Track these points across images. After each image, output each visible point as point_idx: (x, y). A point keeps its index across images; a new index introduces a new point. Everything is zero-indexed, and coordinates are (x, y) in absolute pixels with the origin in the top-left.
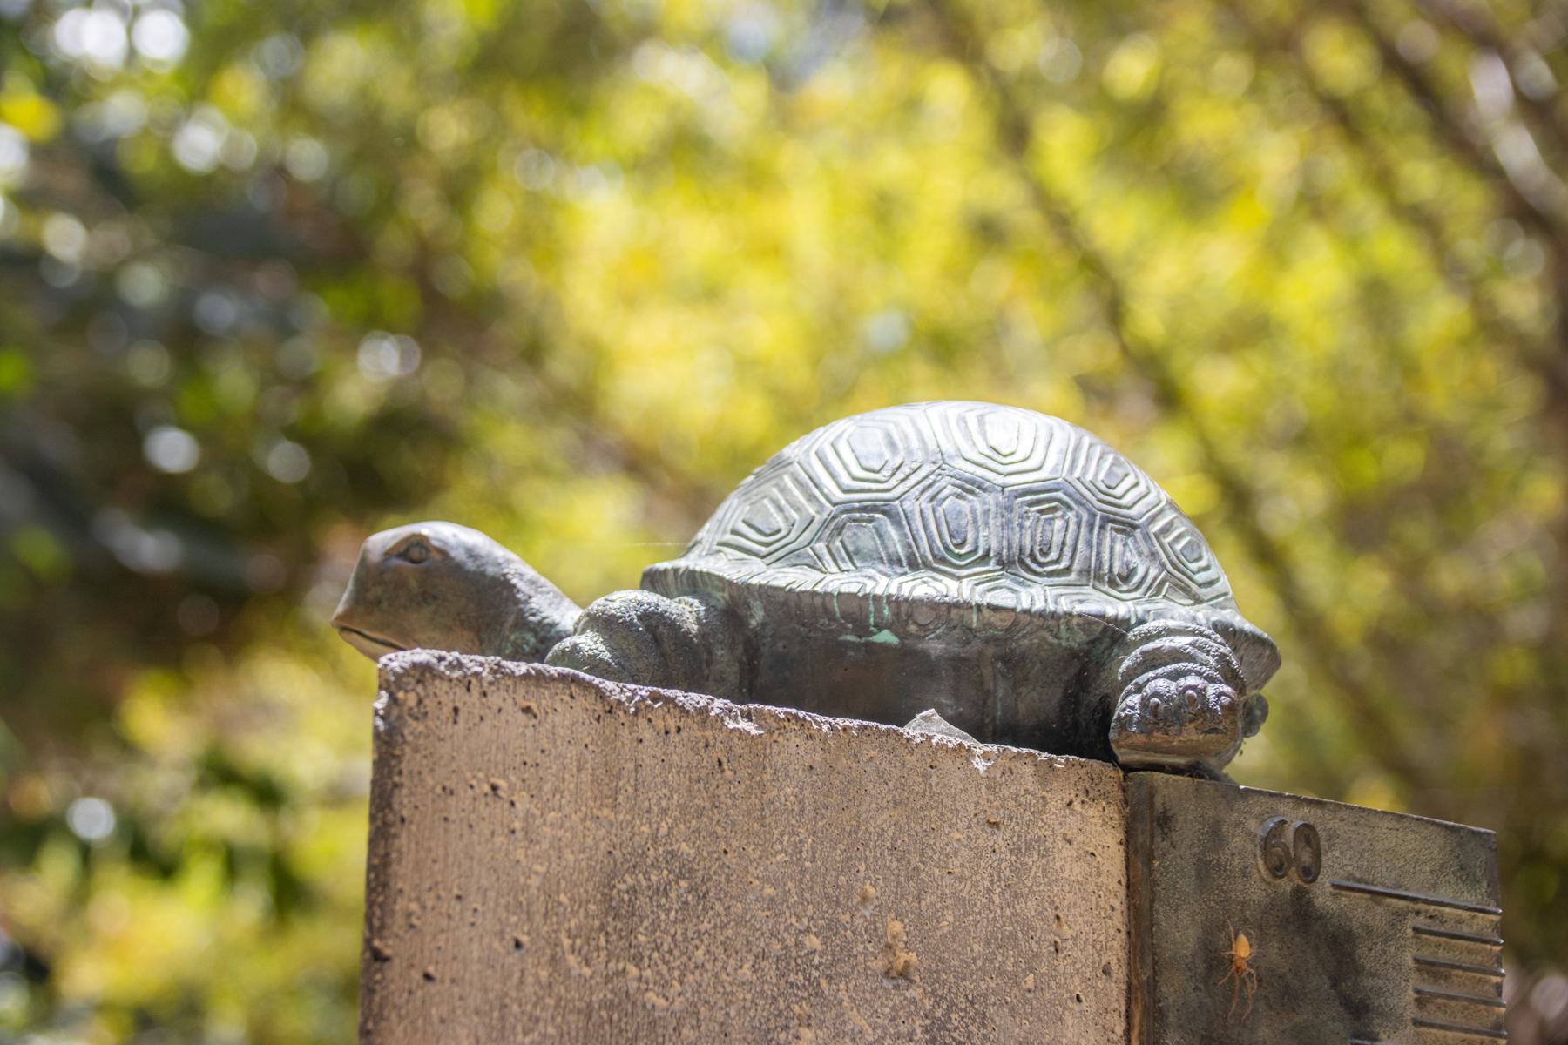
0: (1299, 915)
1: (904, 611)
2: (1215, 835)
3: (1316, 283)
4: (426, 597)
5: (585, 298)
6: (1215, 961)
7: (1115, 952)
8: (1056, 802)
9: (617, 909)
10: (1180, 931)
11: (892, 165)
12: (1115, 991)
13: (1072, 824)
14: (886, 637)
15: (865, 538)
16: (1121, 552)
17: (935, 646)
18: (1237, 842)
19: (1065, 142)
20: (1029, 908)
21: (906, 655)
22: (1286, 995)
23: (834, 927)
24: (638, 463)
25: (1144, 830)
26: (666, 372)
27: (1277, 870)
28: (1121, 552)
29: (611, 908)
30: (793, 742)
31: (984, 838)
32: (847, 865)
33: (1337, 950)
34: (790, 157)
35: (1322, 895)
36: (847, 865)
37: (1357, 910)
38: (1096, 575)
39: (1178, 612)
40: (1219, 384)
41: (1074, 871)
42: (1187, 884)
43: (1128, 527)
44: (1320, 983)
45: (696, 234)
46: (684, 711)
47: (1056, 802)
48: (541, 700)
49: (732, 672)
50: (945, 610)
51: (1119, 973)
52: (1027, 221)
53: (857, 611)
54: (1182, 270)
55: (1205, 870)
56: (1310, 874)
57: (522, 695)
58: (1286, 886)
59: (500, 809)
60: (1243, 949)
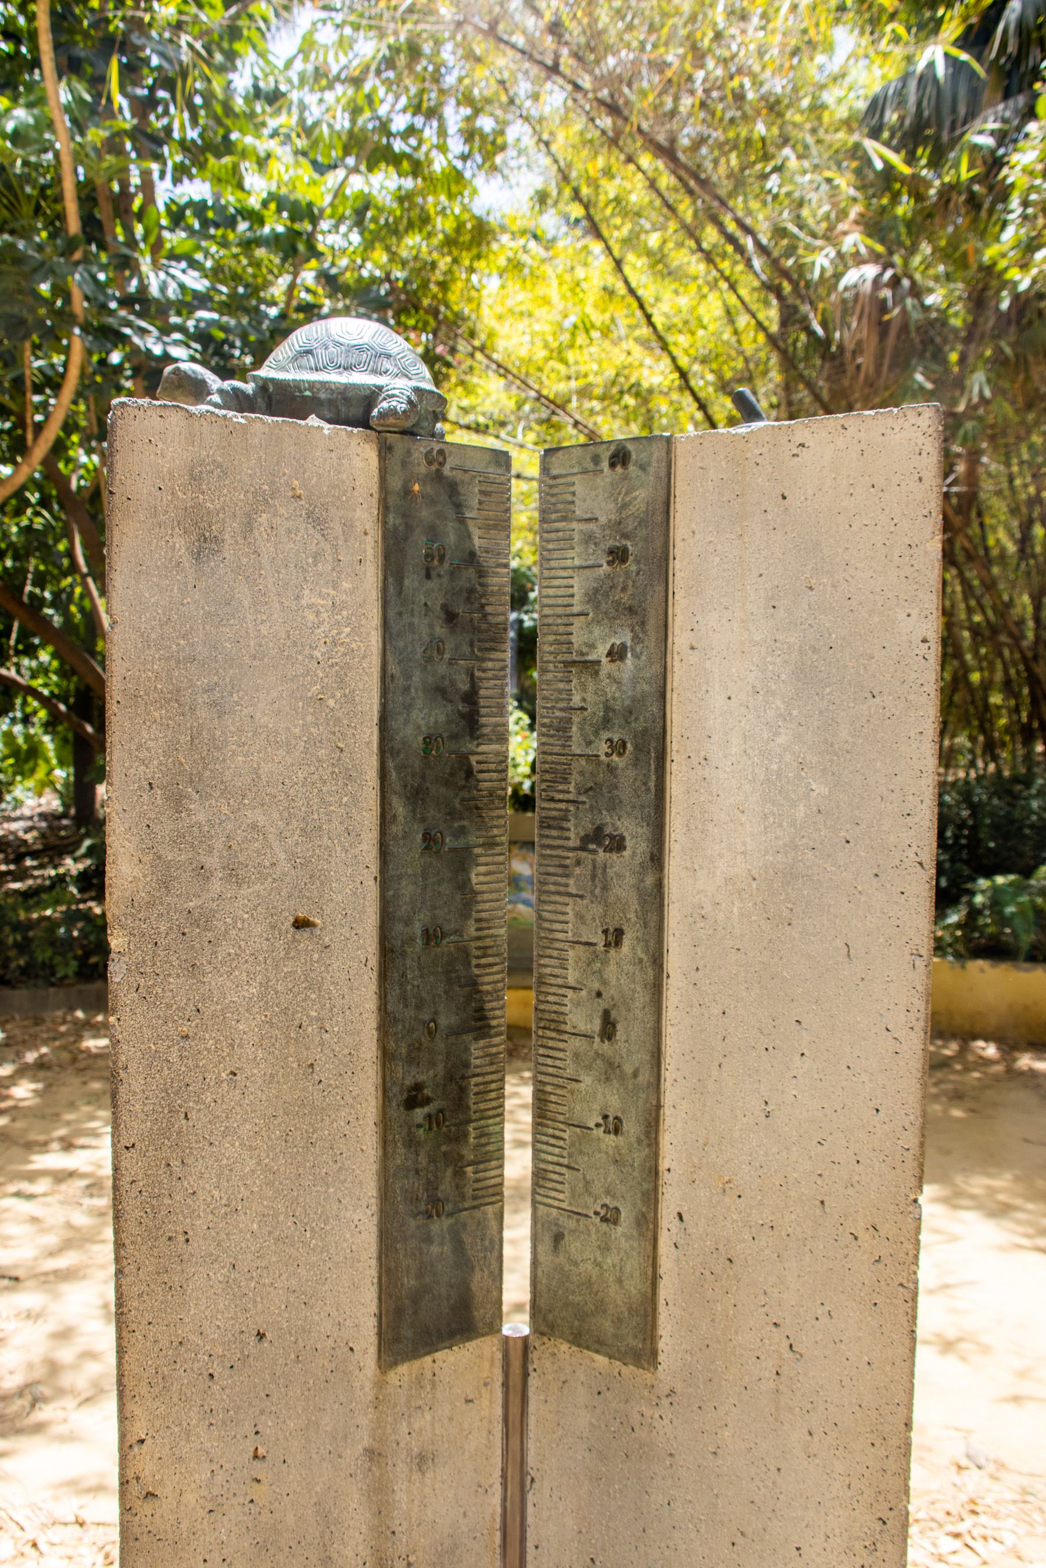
0: (438, 476)
1: (312, 385)
2: (409, 452)
3: (712, 308)
4: (179, 386)
5: (487, 319)
6: (407, 492)
7: (375, 488)
8: (354, 443)
9: (194, 478)
10: (396, 483)
11: (580, 273)
12: (374, 501)
13: (359, 450)
14: (308, 393)
15: (304, 361)
16: (387, 365)
17: (323, 396)
18: (416, 455)
19: (636, 267)
20: (344, 476)
21: (314, 399)
22: (432, 502)
23: (273, 483)
24: (502, 370)
25: (385, 451)
26: (514, 341)
27: (430, 463)
28: (387, 365)
29: (192, 477)
30: (258, 425)
31: (327, 455)
32: (278, 463)
33: (452, 489)
34: (547, 269)
35: (446, 471)
36: (278, 463)
37: (459, 476)
38: (375, 372)
39: (401, 383)
40: (680, 342)
41: (361, 465)
42: (398, 468)
43: (389, 356)
44: (444, 498)
45: (519, 296)
46: (191, 415)
47: (354, 443)
48: (166, 413)
49: (263, 406)
50: (323, 384)
51: (376, 496)
52: (621, 289)
53: (297, 385)
54: (668, 303)
55: (404, 464)
56: (442, 464)
57: (160, 412)
58: (433, 468)
59: (152, 447)
60: (417, 487)
